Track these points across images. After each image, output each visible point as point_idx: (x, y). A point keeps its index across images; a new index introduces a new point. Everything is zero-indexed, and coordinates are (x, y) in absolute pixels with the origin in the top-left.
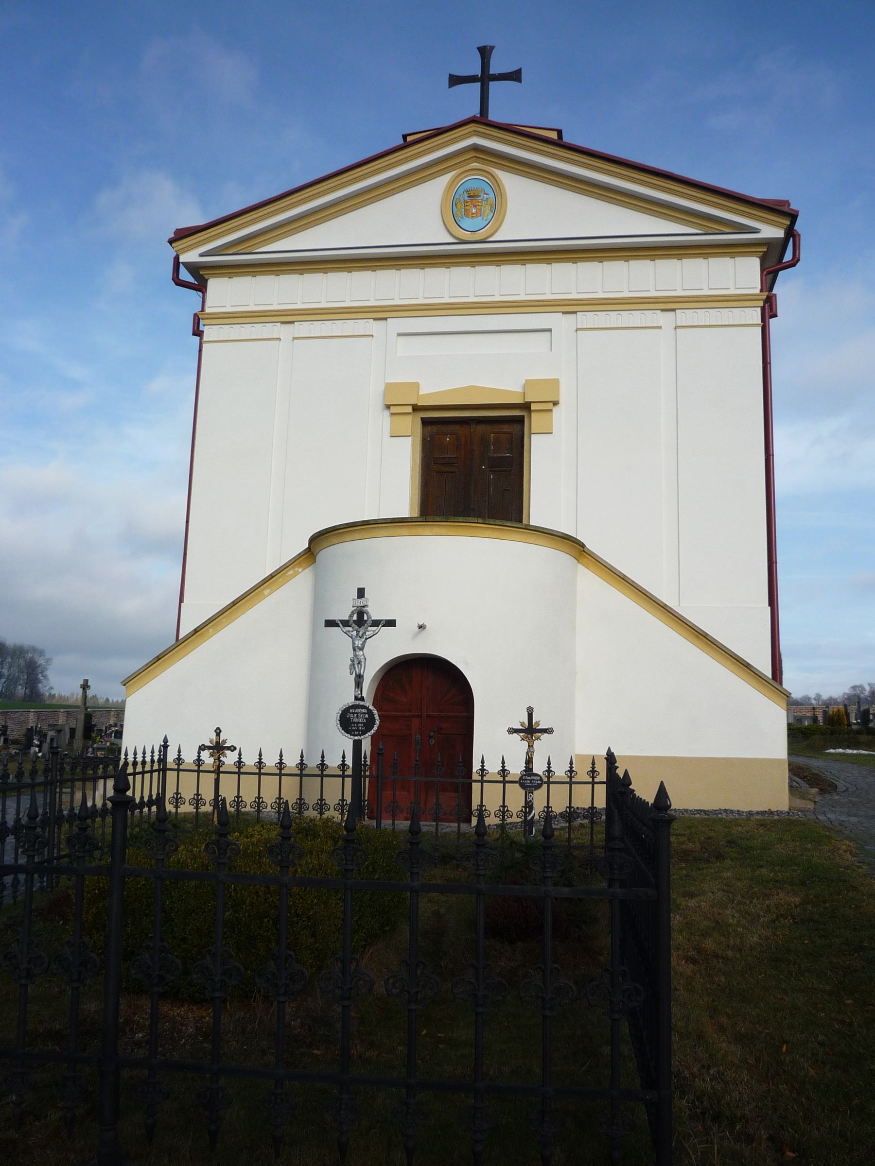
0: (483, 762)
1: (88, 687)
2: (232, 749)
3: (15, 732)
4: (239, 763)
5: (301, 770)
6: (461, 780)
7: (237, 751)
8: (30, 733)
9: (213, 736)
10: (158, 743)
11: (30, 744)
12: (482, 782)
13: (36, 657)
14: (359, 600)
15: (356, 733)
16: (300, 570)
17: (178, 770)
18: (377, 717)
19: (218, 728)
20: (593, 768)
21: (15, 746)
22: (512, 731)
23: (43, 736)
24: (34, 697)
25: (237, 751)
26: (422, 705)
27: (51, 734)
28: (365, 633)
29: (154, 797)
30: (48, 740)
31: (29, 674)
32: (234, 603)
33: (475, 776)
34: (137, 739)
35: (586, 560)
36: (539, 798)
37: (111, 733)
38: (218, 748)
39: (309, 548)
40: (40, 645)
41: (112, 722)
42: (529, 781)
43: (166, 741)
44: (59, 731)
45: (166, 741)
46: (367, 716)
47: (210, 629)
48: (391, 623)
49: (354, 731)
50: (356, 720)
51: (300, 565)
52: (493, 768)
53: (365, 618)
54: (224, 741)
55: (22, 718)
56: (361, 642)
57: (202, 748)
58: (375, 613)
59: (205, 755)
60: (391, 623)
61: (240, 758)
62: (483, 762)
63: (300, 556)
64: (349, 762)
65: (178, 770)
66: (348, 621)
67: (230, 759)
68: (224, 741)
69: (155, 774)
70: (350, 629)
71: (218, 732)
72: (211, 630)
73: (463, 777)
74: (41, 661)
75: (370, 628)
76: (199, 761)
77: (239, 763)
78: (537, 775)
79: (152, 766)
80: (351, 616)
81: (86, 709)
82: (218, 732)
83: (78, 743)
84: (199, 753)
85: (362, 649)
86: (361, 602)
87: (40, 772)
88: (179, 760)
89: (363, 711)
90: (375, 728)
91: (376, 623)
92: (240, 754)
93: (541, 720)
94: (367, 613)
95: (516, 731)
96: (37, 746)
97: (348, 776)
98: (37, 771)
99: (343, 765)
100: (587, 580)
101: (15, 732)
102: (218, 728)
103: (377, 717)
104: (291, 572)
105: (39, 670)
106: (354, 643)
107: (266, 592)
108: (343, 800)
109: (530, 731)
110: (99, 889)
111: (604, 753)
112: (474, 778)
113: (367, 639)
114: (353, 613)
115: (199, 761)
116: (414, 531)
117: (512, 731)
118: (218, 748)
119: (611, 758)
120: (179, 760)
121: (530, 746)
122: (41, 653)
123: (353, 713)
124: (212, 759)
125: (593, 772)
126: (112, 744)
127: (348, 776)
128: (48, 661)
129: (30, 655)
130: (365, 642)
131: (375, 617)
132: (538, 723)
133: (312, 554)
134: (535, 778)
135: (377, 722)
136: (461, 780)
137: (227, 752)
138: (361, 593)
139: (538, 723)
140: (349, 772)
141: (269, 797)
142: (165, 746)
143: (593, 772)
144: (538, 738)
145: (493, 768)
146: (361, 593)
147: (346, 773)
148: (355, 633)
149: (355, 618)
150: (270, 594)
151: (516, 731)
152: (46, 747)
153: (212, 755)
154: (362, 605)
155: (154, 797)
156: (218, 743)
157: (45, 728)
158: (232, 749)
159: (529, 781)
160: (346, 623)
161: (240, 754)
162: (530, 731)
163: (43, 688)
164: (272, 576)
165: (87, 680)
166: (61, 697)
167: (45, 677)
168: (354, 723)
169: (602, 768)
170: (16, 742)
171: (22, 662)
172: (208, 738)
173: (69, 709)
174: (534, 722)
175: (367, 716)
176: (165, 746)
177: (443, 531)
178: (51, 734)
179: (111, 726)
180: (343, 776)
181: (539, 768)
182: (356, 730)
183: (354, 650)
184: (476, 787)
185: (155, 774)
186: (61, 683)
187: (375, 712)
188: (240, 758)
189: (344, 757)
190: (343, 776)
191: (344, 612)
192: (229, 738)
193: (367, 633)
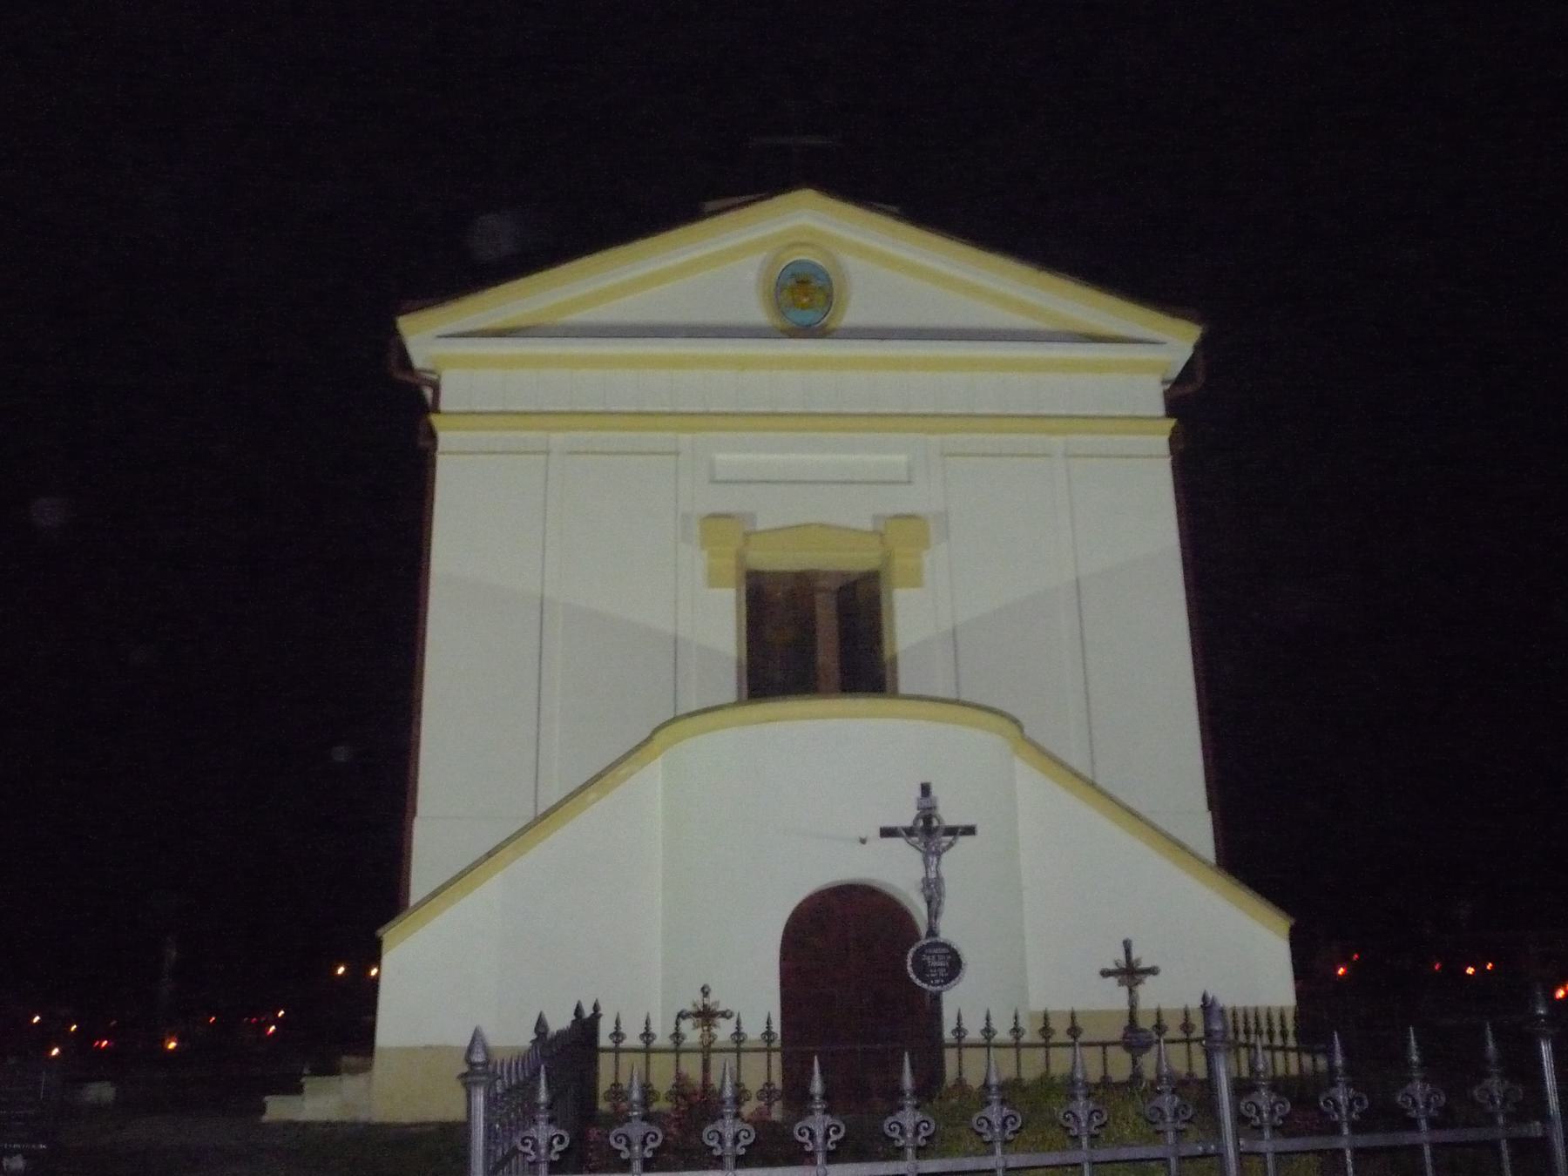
2: (725, 1015)
4: (738, 1035)
5: (738, 1042)
7: (733, 1020)
9: (698, 997)
12: (617, 1051)
25: (733, 1020)
36: (1148, 1062)
38: (706, 1016)
42: (1135, 1038)
47: (506, 853)
48: (970, 831)
50: (935, 964)
53: (935, 823)
54: (717, 1003)
57: (682, 1016)
59: (686, 1026)
60: (970, 831)
61: (738, 1028)
64: (776, 1028)
67: (723, 1031)
71: (705, 991)
76: (677, 1036)
77: (738, 1035)
78: (1144, 1031)
82: (705, 991)
84: (677, 1024)
86: (925, 803)
91: (952, 831)
92: (738, 1022)
97: (775, 1050)
99: (768, 1033)
107: (592, 796)
108: (768, 1084)
109: (1130, 973)
111: (1195, 1003)
114: (917, 818)
115: (677, 1036)
117: (1106, 973)
118: (706, 1016)
121: (1131, 991)
124: (699, 1031)
127: (775, 1050)
132: (1138, 961)
137: (721, 1021)
139: (1138, 961)
140: (777, 1044)
141: (663, 1081)
143: (1187, 1027)
149: (921, 823)
153: (696, 1027)
158: (725, 1015)
159: (1135, 1038)
160: (910, 832)
161: (738, 1022)
162: (1130, 973)
164: (599, 777)
169: (1197, 1021)
172: (690, 1000)
181: (1146, 1023)
184: (950, 1056)
188: (738, 1028)
190: (769, 1050)
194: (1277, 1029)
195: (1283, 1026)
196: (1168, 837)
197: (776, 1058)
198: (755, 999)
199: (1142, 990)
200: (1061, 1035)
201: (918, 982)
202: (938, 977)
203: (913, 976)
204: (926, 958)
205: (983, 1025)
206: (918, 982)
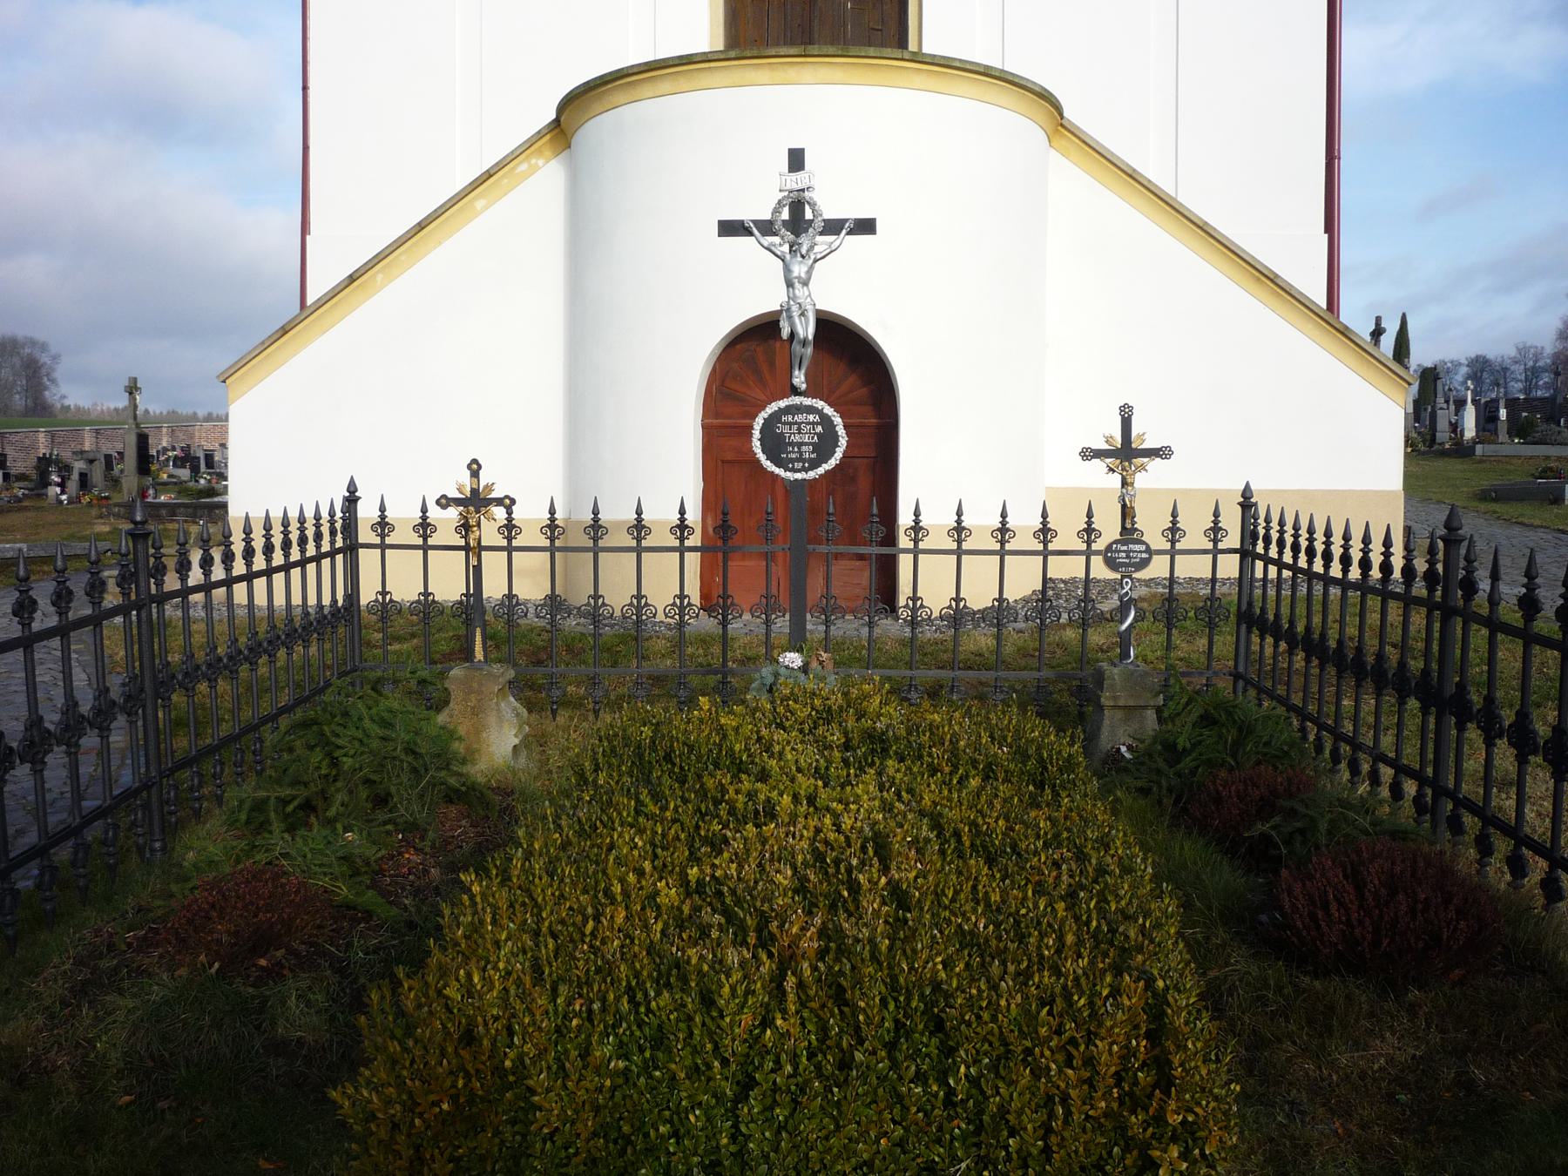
0: (917, 513)
1: (137, 389)
3: (19, 463)
4: (510, 528)
6: (876, 550)
8: (44, 463)
10: (340, 493)
11: (45, 482)
13: (37, 354)
14: (794, 176)
15: (798, 465)
16: (541, 162)
17: (383, 547)
18: (841, 430)
19: (475, 461)
20: (1216, 522)
21: (21, 484)
22: (1090, 454)
23: (65, 470)
24: (39, 409)
26: (808, 412)
27: (79, 466)
28: (811, 248)
29: (340, 603)
30: (75, 476)
31: (28, 379)
32: (421, 226)
33: (904, 542)
34: (268, 482)
35: (1064, 142)
37: (167, 460)
38: (476, 501)
39: (557, 123)
40: (40, 336)
41: (165, 444)
43: (352, 488)
44: (91, 462)
45: (352, 488)
46: (819, 429)
48: (865, 227)
49: (792, 461)
50: (797, 438)
51: (539, 152)
52: (938, 519)
53: (808, 215)
54: (489, 488)
55: (27, 442)
56: (804, 269)
58: (830, 203)
60: (865, 227)
62: (917, 513)
63: (539, 135)
64: (694, 516)
65: (383, 547)
66: (770, 223)
68: (489, 488)
69: (339, 558)
70: (776, 240)
71: (475, 468)
72: (380, 277)
73: (882, 544)
74: (44, 359)
75: (819, 239)
79: (333, 542)
80: (777, 211)
81: (137, 426)
82: (475, 468)
83: (130, 481)
85: (805, 283)
86: (796, 181)
87: (112, 586)
88: (383, 525)
89: (811, 417)
90: (839, 454)
91: (833, 227)
93: (1147, 433)
94: (813, 205)
95: (1098, 454)
96: (58, 485)
97: (693, 549)
98: (103, 583)
99: (682, 527)
100: (1067, 177)
101: (19, 463)
102: (475, 461)
103: (841, 430)
104: (524, 167)
105: (44, 371)
106: (787, 270)
107: (480, 204)
108: (682, 596)
109: (1126, 453)
110: (454, 1099)
112: (901, 546)
113: (816, 261)
115: (424, 527)
116: (780, 74)
118: (476, 501)
119: (1247, 504)
120: (383, 525)
122: (44, 347)
123: (790, 424)
125: (1216, 531)
126: (170, 476)
127: (693, 549)
128: (55, 358)
129: (27, 350)
130: (811, 268)
131: (829, 214)
133: (562, 131)
134: (1137, 547)
135: (843, 442)
136: (876, 550)
138: (796, 160)
139: (1141, 436)
140: (694, 540)
142: (351, 500)
143: (1216, 531)
144: (1143, 468)
145: (938, 519)
146: (796, 160)
147: (687, 543)
148: (786, 248)
149: (785, 214)
150: (486, 208)
151: (1098, 454)
152: (73, 485)
154: (800, 186)
155: (340, 603)
156: (475, 492)
157: (66, 455)
160: (766, 228)
162: (1126, 453)
163: (52, 396)
164: (488, 175)
165: (135, 380)
166: (78, 408)
167: (53, 381)
168: (792, 444)
169: (1232, 522)
170: (22, 477)
171: (16, 361)
172: (456, 482)
173: (102, 425)
174: (1134, 434)
175: (819, 429)
176: (351, 500)
177: (838, 74)
178: (79, 466)
179: (165, 450)
180: (682, 550)
182: (797, 460)
183: (790, 284)
185: (339, 558)
186: (83, 389)
187: (838, 420)
189: (682, 512)
190: (682, 550)
191: (760, 206)
192: (496, 479)
193: (817, 249)
194: (1337, 551)
195: (1346, 547)
196: (1205, 230)
197: (693, 560)
198: (666, 476)
199: (1141, 481)
200: (1024, 540)
201: (769, 465)
202: (800, 459)
203: (762, 457)
204: (781, 429)
205: (1037, 523)
206: (769, 465)
